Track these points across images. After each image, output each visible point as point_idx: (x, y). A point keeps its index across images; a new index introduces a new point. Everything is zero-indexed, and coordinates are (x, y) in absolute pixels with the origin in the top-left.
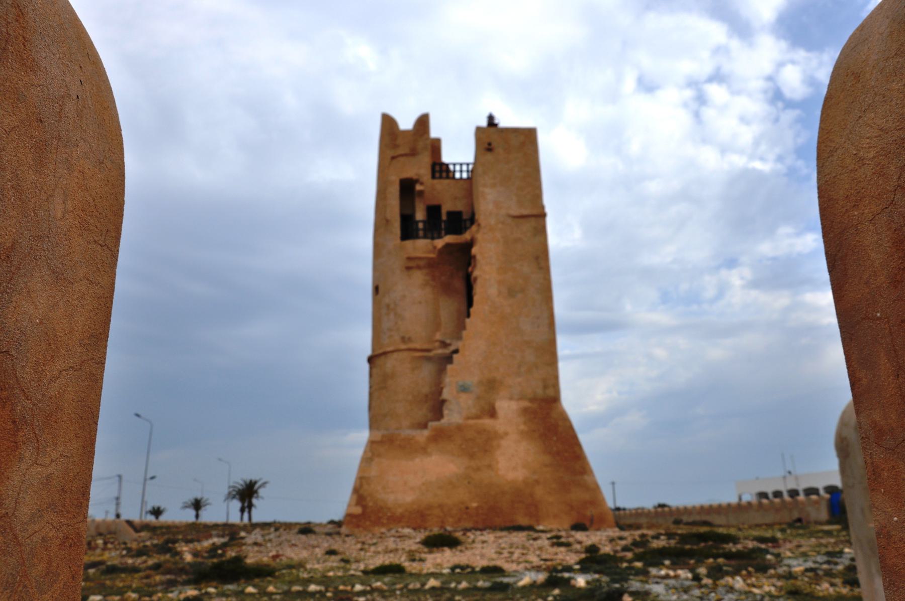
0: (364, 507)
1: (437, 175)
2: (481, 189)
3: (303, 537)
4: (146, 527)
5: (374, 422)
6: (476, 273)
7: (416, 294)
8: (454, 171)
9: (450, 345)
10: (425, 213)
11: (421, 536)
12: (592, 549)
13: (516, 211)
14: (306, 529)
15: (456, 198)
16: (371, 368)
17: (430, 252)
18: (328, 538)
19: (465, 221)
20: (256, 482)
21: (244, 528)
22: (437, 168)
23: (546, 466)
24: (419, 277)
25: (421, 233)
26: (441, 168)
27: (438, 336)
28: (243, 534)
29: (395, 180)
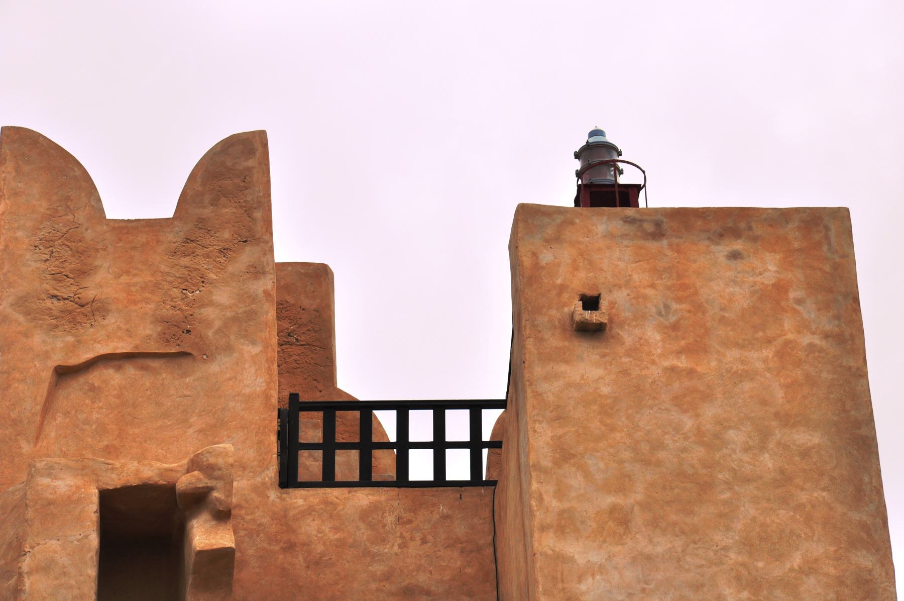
1: (310, 464)
2: (546, 543)
8: (403, 445)
22: (311, 429)
26: (329, 428)
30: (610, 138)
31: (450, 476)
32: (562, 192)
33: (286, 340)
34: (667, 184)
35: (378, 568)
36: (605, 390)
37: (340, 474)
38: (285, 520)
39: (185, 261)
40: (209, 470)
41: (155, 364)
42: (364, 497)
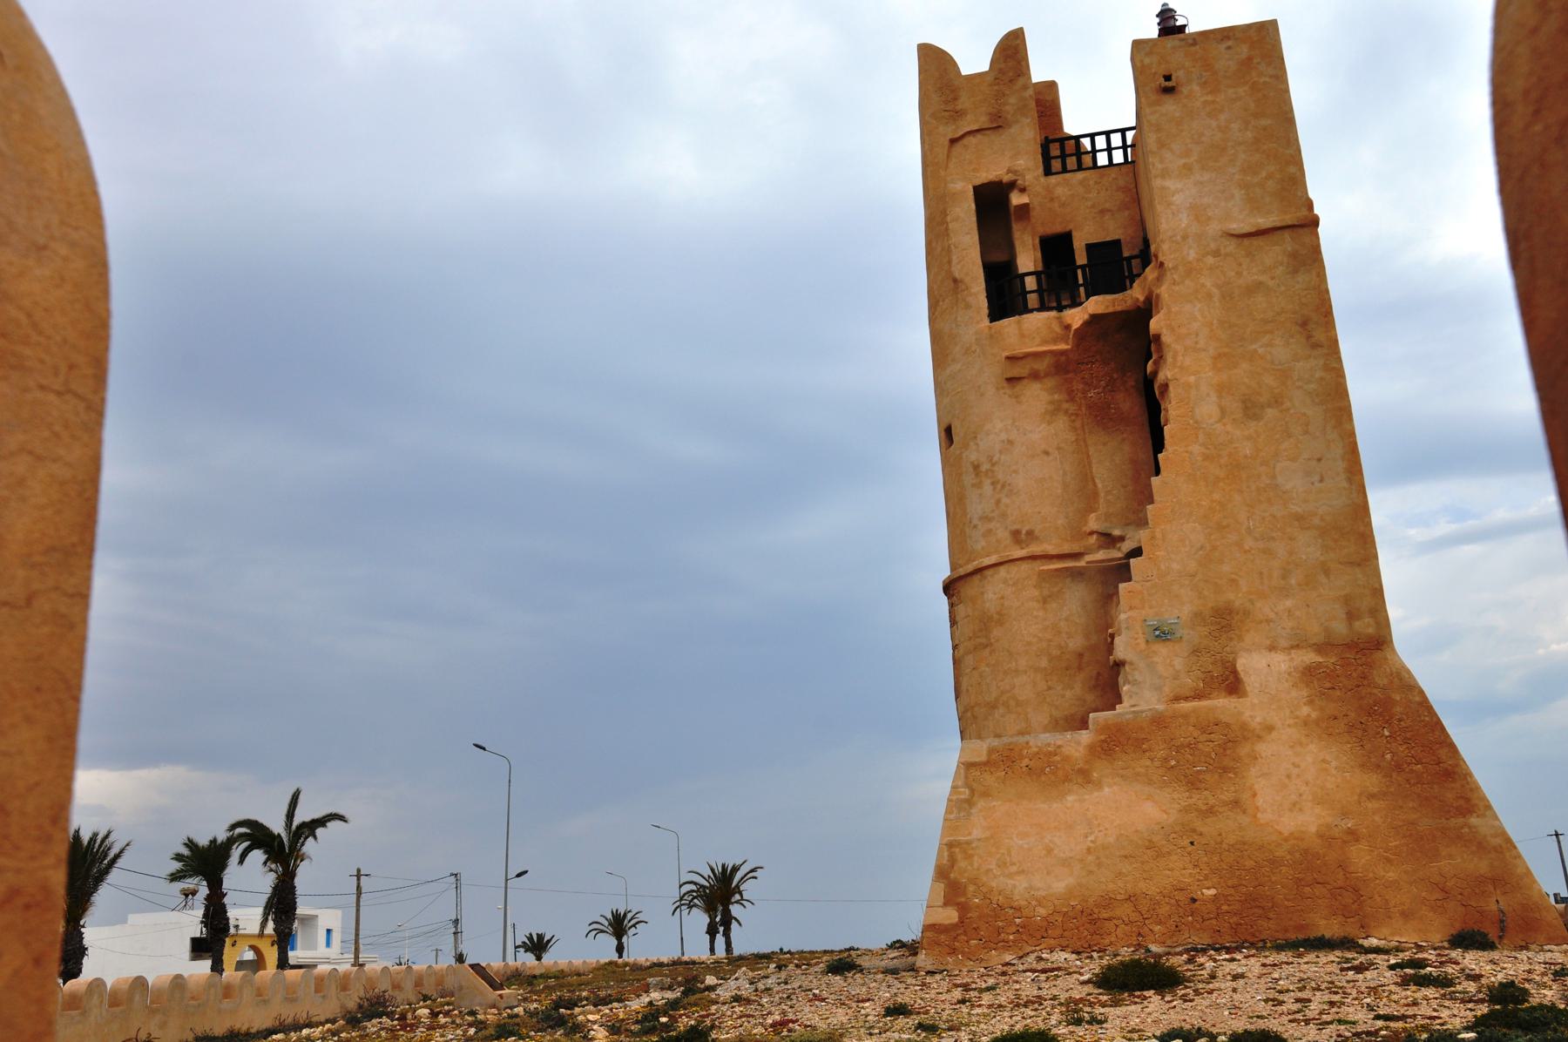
0: (963, 909)
1: (1056, 165)
2: (1157, 183)
3: (837, 979)
4: (516, 977)
5: (969, 724)
7: (1035, 438)
8: (1094, 151)
9: (1122, 539)
11: (1093, 967)
12: (1507, 994)
14: (843, 965)
15: (1103, 212)
16: (952, 605)
17: (1055, 341)
18: (889, 978)
19: (1129, 259)
20: (735, 869)
21: (716, 968)
22: (1055, 150)
23: (1372, 797)
24: (1037, 396)
25: (1033, 300)
26: (1062, 148)
27: (1093, 523)
28: (710, 980)
29: (963, 190)
32: (1152, 31)
33: (1041, 115)
34: (1196, 20)
37: (1069, 167)
38: (1049, 190)
40: (1015, 172)
42: (1080, 175)
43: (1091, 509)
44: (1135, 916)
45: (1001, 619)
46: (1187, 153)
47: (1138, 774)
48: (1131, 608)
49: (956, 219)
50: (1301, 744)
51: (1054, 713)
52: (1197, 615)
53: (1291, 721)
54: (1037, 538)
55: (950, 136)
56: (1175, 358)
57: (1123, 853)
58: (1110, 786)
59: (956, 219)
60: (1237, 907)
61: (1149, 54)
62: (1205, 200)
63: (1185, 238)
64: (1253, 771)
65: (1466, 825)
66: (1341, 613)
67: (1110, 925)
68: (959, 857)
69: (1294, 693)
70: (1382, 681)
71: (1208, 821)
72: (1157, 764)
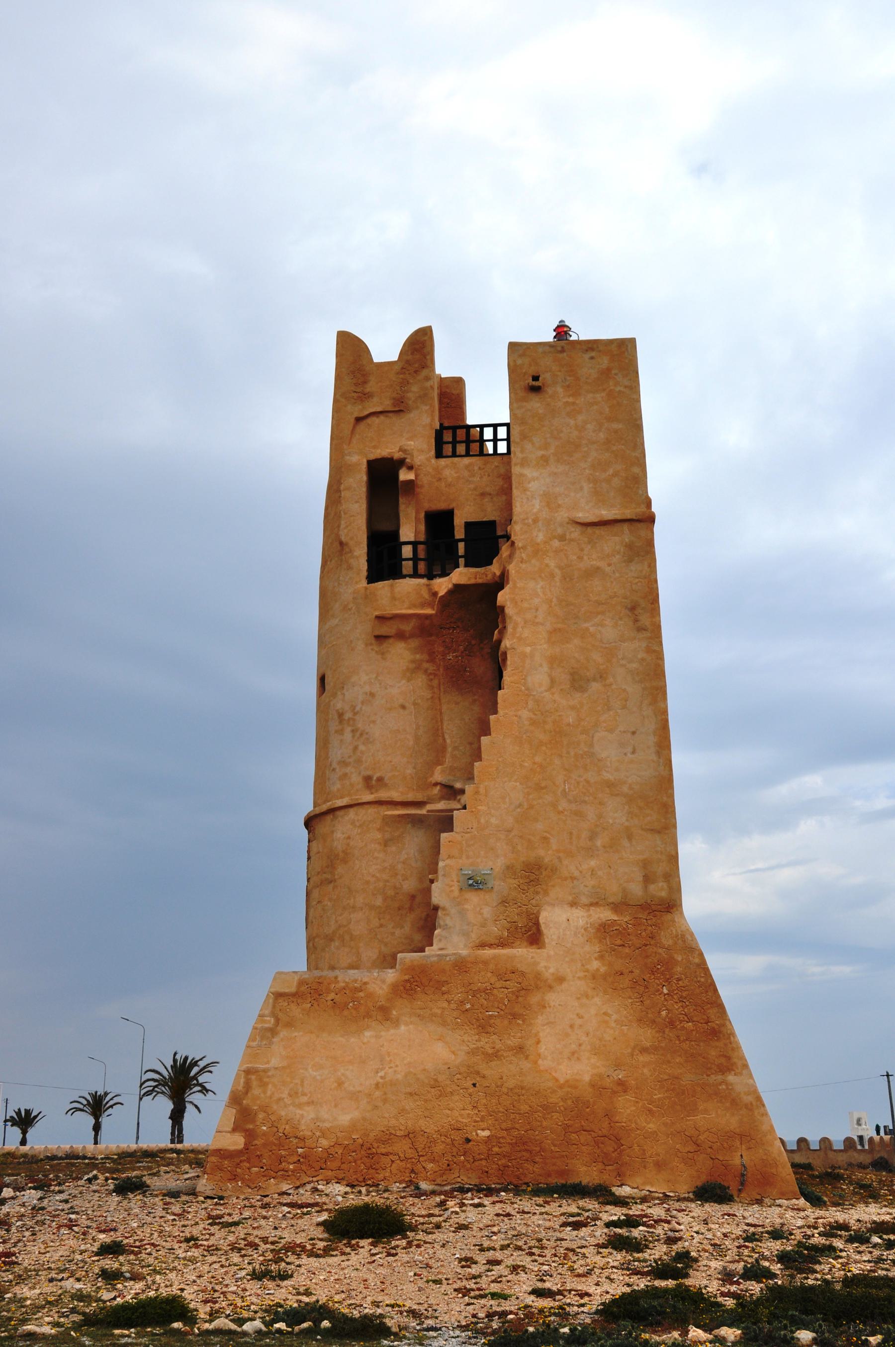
0: (250, 1135)
1: (448, 449)
6: (507, 643)
7: (394, 689)
10: (422, 527)
13: (584, 515)
15: (483, 495)
17: (423, 605)
22: (448, 436)
23: (644, 1050)
24: (401, 654)
26: (454, 436)
27: (438, 775)
29: (359, 460)
30: (567, 323)
31: (499, 451)
35: (472, 486)
36: (541, 411)
38: (438, 470)
39: (401, 376)
41: (390, 415)
42: (467, 461)
43: (439, 762)
44: (410, 1153)
45: (346, 857)
46: (546, 446)
47: (435, 1015)
48: (449, 857)
49: (348, 489)
50: (587, 996)
51: (383, 949)
52: (509, 868)
53: (581, 974)
54: (386, 785)
55: (356, 415)
56: (515, 628)
57: (408, 1090)
58: (406, 1024)
59: (348, 489)
60: (507, 1149)
61: (522, 355)
62: (557, 490)
63: (535, 521)
64: (540, 1020)
65: (724, 1082)
66: (639, 876)
67: (386, 1160)
68: (255, 1083)
69: (587, 948)
70: (667, 942)
71: (493, 1064)
72: (453, 1006)
